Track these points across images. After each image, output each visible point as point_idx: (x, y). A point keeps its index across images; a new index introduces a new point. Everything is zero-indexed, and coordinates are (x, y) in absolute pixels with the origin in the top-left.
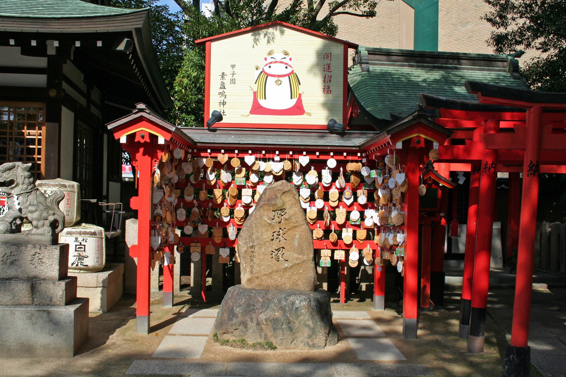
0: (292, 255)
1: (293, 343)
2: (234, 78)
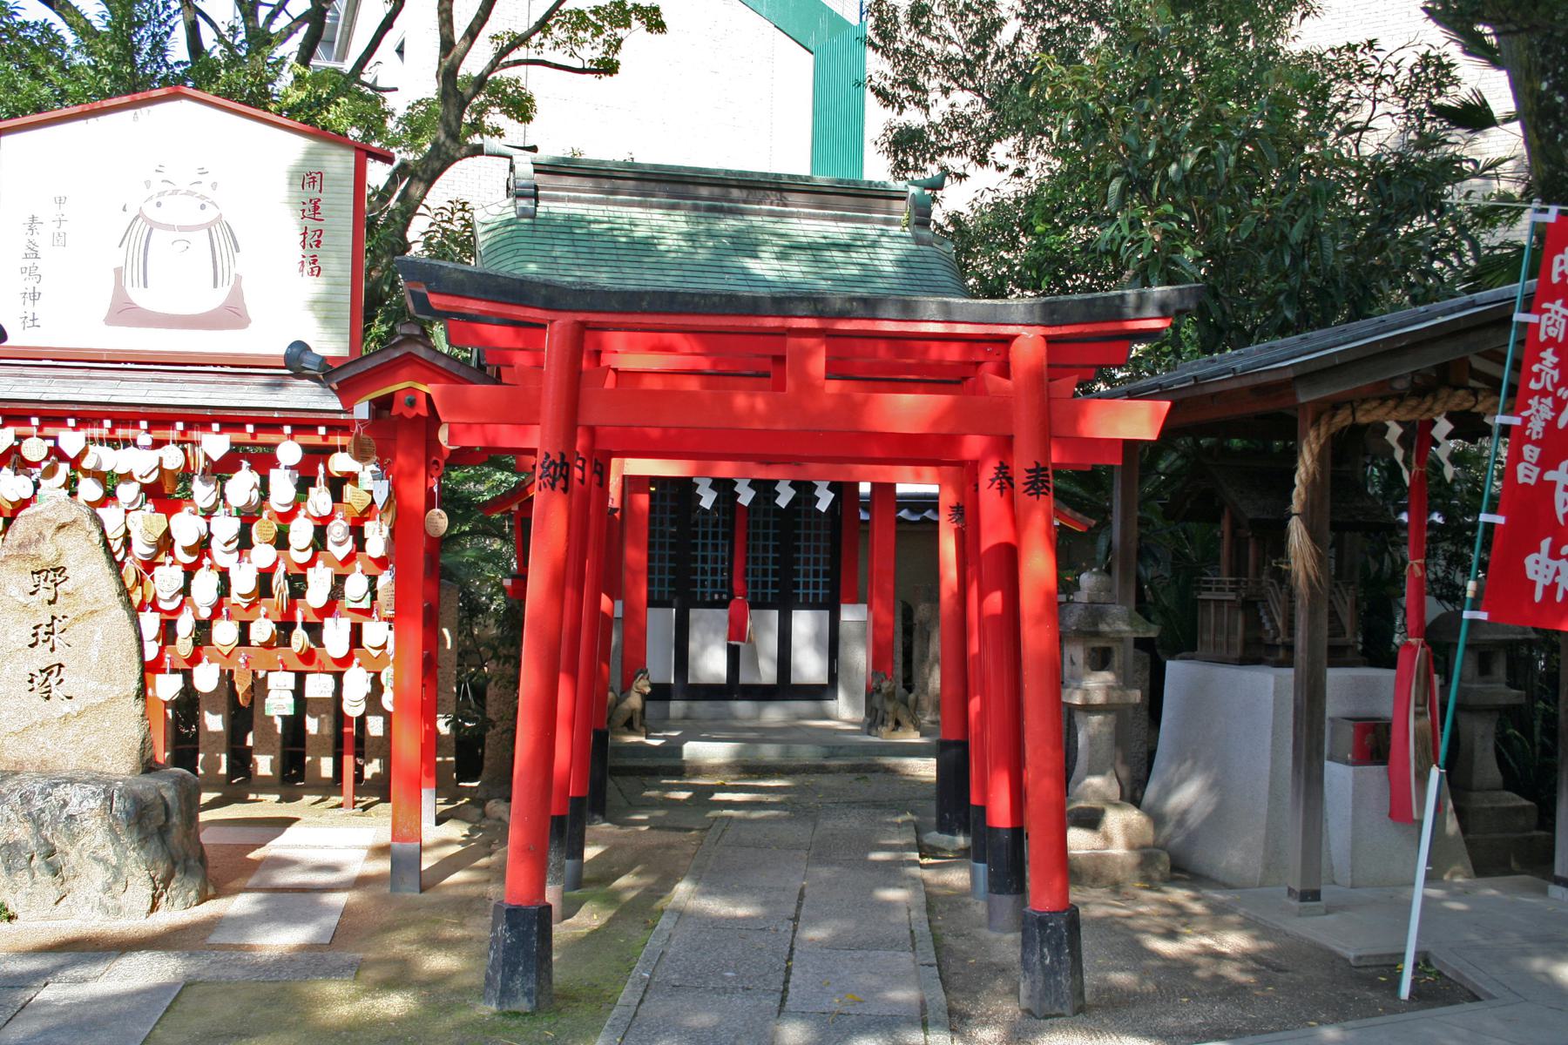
2: (62, 230)
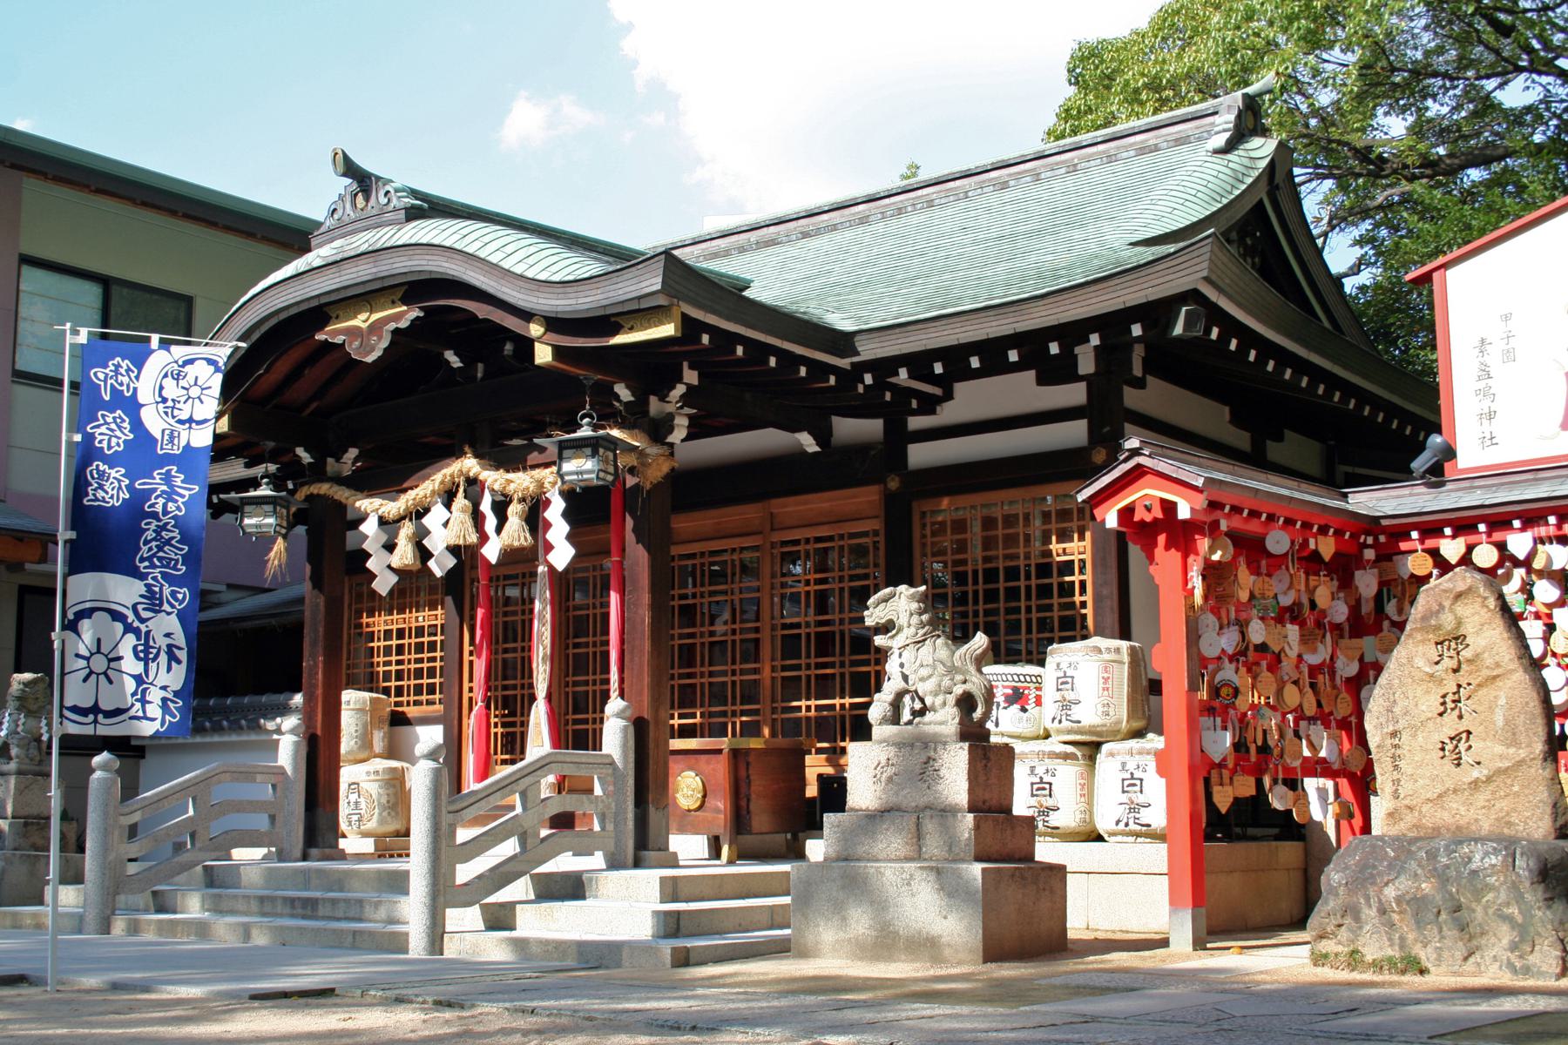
0: (1488, 751)
1: (1472, 960)
